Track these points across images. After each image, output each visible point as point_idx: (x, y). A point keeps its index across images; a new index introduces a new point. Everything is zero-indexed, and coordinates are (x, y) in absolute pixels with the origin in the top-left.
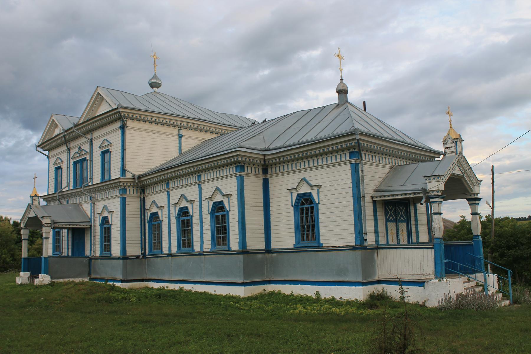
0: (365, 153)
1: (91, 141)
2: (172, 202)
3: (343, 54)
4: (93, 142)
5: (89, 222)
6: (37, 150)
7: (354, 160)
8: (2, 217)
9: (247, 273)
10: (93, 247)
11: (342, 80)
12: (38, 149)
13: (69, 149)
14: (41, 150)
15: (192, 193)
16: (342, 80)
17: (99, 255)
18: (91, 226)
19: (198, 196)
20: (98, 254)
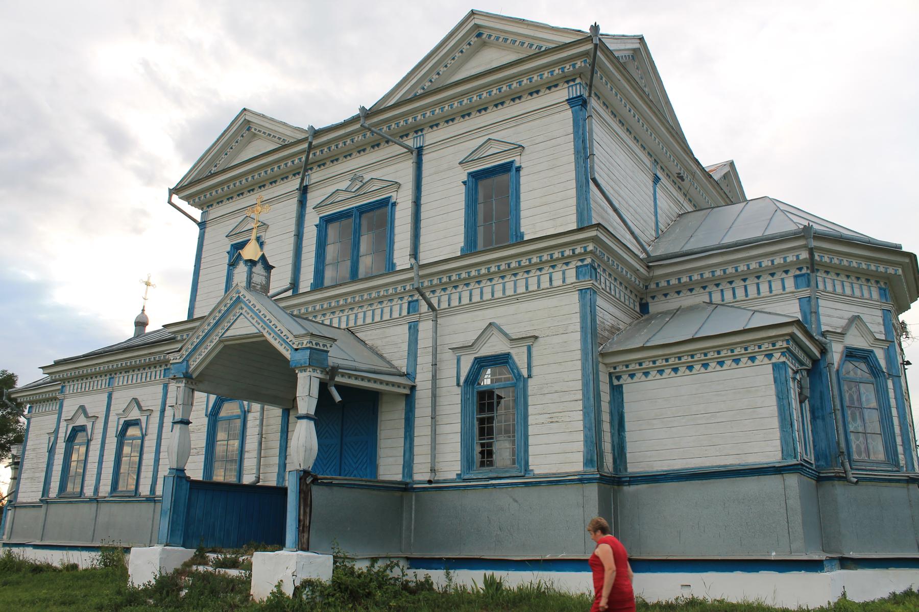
0: (824, 275)
1: (420, 151)
2: (63, 417)
3: (152, 281)
4: (425, 158)
5: (406, 375)
6: (170, 202)
7: (805, 292)
8: (10, 380)
9: (822, 524)
10: (437, 446)
11: (143, 310)
12: (175, 199)
13: (304, 190)
14: (184, 205)
15: (96, 403)
16: (143, 310)
17: (509, 462)
18: (413, 388)
19: (160, 402)
20: (451, 465)
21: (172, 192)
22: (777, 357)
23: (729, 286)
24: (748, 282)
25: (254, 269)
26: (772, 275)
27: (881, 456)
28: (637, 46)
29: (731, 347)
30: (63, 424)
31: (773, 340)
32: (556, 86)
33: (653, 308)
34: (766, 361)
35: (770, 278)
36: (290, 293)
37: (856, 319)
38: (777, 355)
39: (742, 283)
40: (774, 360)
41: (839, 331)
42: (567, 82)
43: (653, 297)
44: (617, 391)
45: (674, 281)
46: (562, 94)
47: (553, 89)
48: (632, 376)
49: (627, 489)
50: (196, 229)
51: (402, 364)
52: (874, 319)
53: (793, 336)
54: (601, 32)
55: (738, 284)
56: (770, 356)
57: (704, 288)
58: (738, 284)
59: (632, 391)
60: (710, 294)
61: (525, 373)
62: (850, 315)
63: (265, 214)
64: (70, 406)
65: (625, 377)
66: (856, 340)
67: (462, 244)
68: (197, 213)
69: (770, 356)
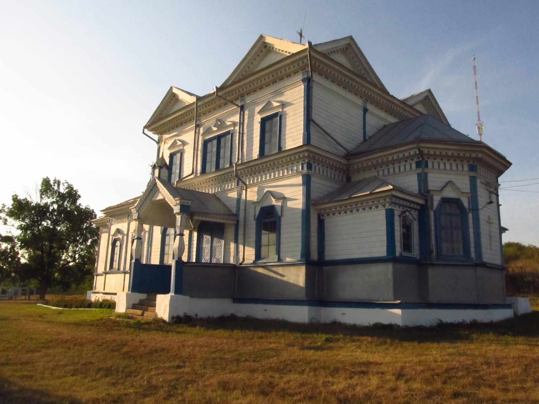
6: (143, 133)
12: (146, 131)
14: (150, 133)
21: (145, 127)
22: (387, 206)
23: (386, 167)
24: (395, 165)
25: (162, 170)
26: (406, 161)
27: (462, 253)
28: (348, 41)
29: (367, 201)
30: (111, 237)
31: (385, 198)
32: (298, 72)
33: (355, 178)
34: (383, 208)
35: (405, 163)
36: (192, 176)
37: (450, 183)
38: (387, 205)
39: (392, 166)
40: (387, 207)
41: (439, 189)
42: (302, 70)
43: (353, 174)
44: (321, 223)
45: (385, 160)
46: (300, 77)
47: (297, 74)
48: (328, 215)
49: (325, 268)
50: (156, 146)
51: (234, 211)
52: (463, 182)
53: (393, 196)
54: (313, 44)
55: (391, 166)
56: (384, 206)
57: (375, 168)
58: (391, 166)
59: (329, 222)
60: (378, 171)
61: (280, 214)
62: (447, 180)
63: (184, 137)
64: (113, 229)
65: (325, 215)
66: (449, 193)
67: (258, 153)
68: (156, 137)
69: (384, 206)
